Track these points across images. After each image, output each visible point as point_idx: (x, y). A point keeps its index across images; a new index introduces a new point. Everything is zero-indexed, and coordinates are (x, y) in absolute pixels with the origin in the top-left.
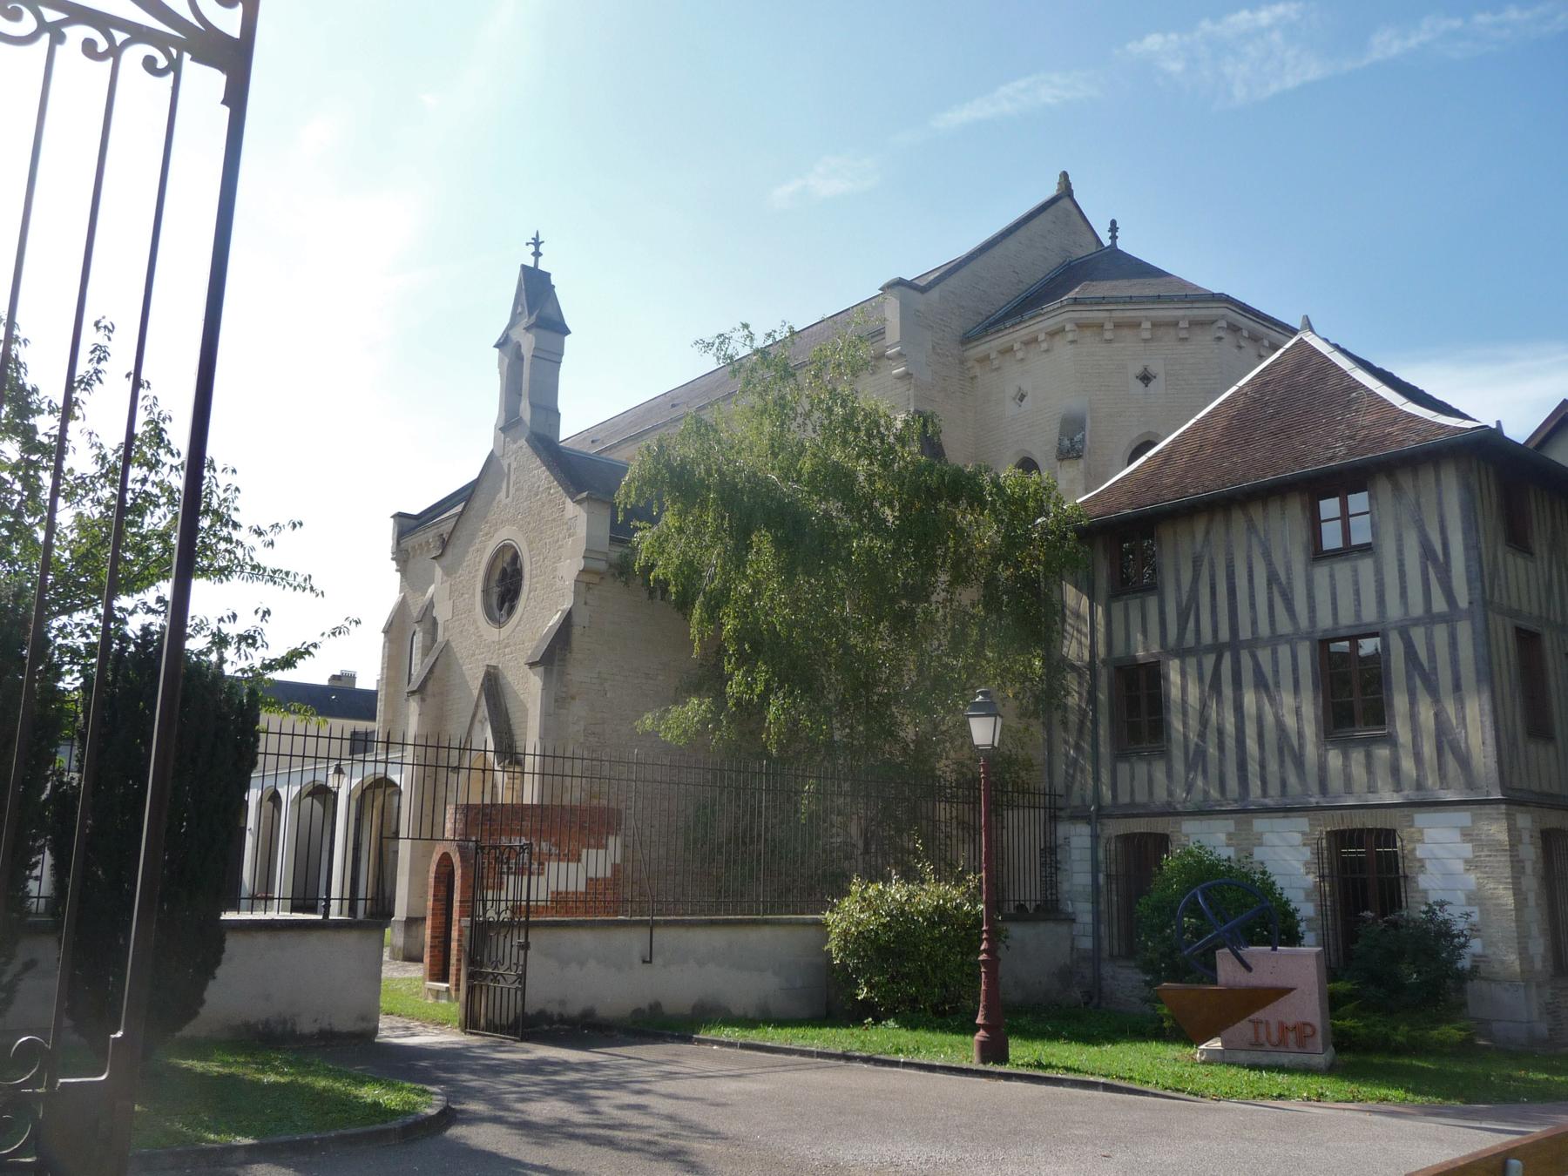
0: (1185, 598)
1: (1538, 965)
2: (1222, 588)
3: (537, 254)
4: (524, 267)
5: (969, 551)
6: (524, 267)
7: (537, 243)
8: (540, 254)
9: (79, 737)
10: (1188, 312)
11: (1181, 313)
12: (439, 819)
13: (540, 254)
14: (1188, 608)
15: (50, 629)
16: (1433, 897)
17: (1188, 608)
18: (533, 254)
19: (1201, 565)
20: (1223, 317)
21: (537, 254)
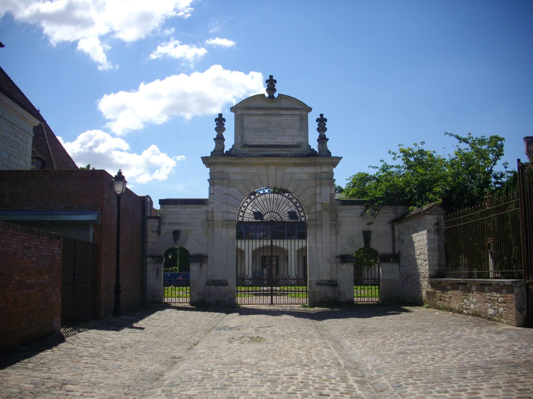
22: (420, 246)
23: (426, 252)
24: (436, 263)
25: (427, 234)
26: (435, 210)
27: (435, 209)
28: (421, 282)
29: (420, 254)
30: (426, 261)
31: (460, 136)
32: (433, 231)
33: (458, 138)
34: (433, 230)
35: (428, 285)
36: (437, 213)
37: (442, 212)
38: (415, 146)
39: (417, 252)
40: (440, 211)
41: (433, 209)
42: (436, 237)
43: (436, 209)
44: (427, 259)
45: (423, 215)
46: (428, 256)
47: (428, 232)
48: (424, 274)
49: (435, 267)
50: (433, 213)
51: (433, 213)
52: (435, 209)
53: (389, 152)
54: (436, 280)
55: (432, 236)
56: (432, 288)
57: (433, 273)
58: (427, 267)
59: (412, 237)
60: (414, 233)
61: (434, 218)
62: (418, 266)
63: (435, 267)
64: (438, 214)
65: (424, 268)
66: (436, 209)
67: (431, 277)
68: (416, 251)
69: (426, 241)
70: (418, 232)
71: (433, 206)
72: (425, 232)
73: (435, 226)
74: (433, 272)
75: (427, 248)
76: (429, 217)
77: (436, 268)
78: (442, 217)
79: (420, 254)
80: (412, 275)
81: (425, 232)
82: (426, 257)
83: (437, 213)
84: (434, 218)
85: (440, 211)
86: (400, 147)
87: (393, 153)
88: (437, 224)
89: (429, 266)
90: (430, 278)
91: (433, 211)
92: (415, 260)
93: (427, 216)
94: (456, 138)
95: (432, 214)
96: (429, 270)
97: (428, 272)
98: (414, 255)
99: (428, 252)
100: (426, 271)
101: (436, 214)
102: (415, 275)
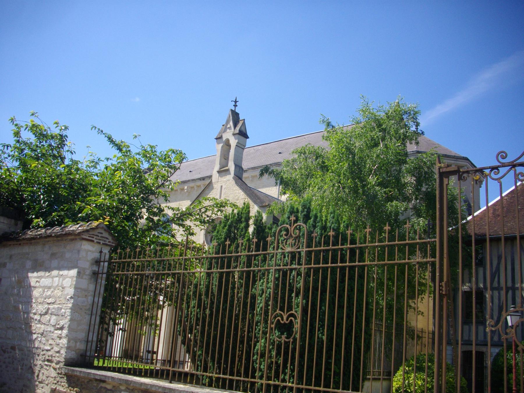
0: (494, 269)
1: (5, 222)
2: (509, 267)
3: (235, 106)
4: (232, 110)
5: (310, 170)
6: (232, 110)
7: (236, 102)
8: (237, 106)
9: (262, 370)
10: (455, 162)
11: (453, 162)
12: (129, 327)
13: (237, 106)
14: (495, 273)
15: (286, 334)
16: (421, 328)
17: (495, 273)
18: (234, 105)
19: (501, 259)
20: (466, 165)
21: (235, 106)
22: (49, 297)
23: (68, 312)
24: (82, 335)
25: (77, 277)
26: (100, 235)
27: (99, 233)
28: (37, 369)
29: (46, 313)
30: (62, 328)
31: (114, 138)
32: (87, 273)
33: (110, 140)
34: (88, 272)
35: (58, 379)
36: (102, 242)
37: (109, 242)
38: (55, 125)
39: (38, 308)
40: (107, 239)
41: (96, 232)
42: (92, 287)
43: (102, 233)
44: (66, 326)
45: (72, 240)
46: (71, 320)
47: (79, 273)
48: (50, 353)
49: (78, 344)
50: (95, 241)
51: (95, 241)
52: (99, 233)
53: (12, 120)
54: (73, 371)
55: (85, 283)
56: (69, 386)
57: (73, 355)
58: (64, 341)
59: (28, 277)
60: (35, 269)
61: (94, 249)
62: (35, 336)
63: (78, 344)
64: (103, 244)
65: (51, 342)
66: (102, 233)
67: (69, 363)
68: (34, 305)
69: (71, 291)
70: (48, 269)
71: (97, 227)
72: (73, 272)
73: (92, 264)
74: (73, 352)
75: (70, 305)
76: (86, 246)
77: (81, 346)
78: (106, 250)
79: (46, 313)
80: (13, 348)
81: (73, 272)
82: (65, 322)
83: (102, 242)
84: (94, 249)
85: (107, 239)
86: (33, 118)
87: (16, 125)
88: (97, 262)
89: (69, 341)
90: (65, 365)
91: (95, 237)
92: (28, 324)
93: (84, 242)
94: (107, 139)
95: (93, 241)
96: (68, 348)
97: (63, 352)
98: (28, 313)
99: (71, 312)
100: (56, 349)
101: (99, 243)
102: (19, 350)
